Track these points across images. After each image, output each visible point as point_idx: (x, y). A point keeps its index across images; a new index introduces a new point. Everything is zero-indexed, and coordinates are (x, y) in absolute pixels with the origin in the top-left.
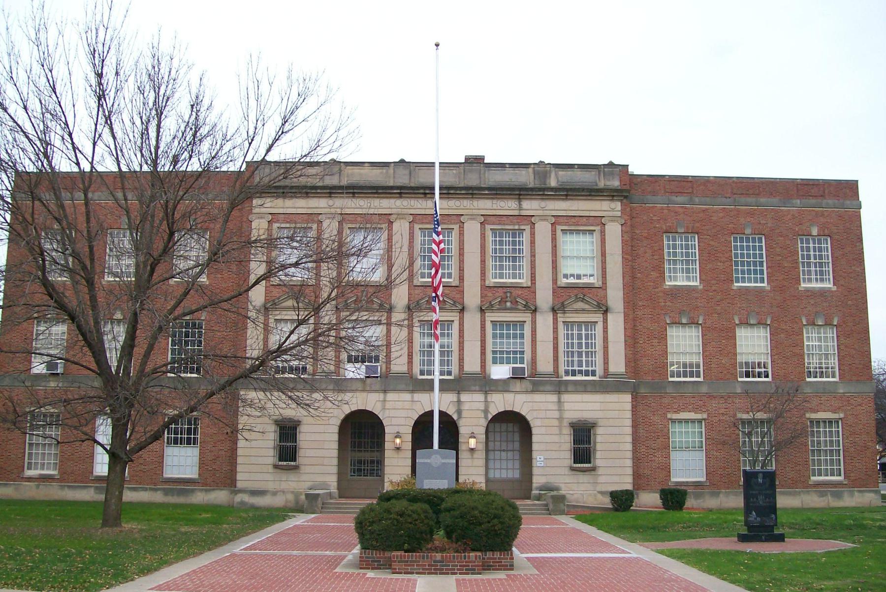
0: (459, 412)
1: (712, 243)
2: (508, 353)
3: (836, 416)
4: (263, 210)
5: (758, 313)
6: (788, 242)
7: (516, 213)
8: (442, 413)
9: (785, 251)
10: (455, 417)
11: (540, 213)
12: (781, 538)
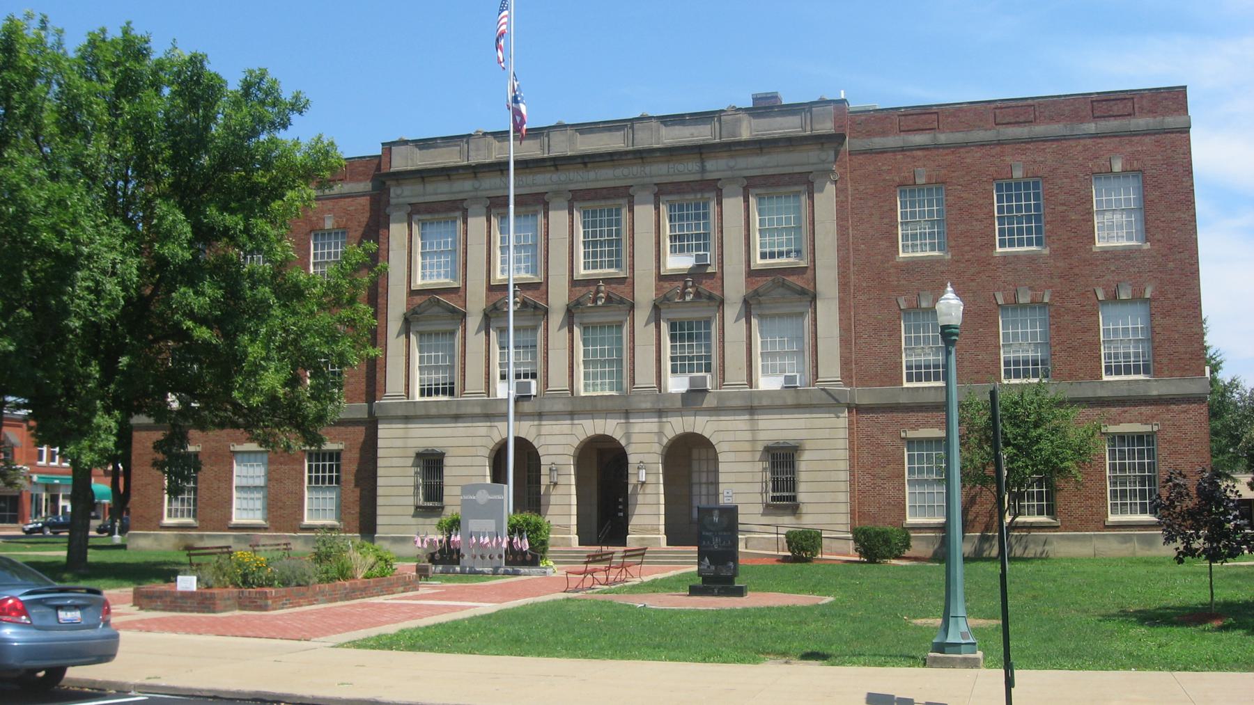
0: (628, 435)
1: (964, 195)
2: (691, 359)
3: (1147, 428)
4: (401, 200)
5: (1031, 288)
6: (1077, 185)
7: (698, 177)
8: (518, 440)
9: (1072, 199)
10: (623, 442)
11: (729, 174)
12: (740, 592)
